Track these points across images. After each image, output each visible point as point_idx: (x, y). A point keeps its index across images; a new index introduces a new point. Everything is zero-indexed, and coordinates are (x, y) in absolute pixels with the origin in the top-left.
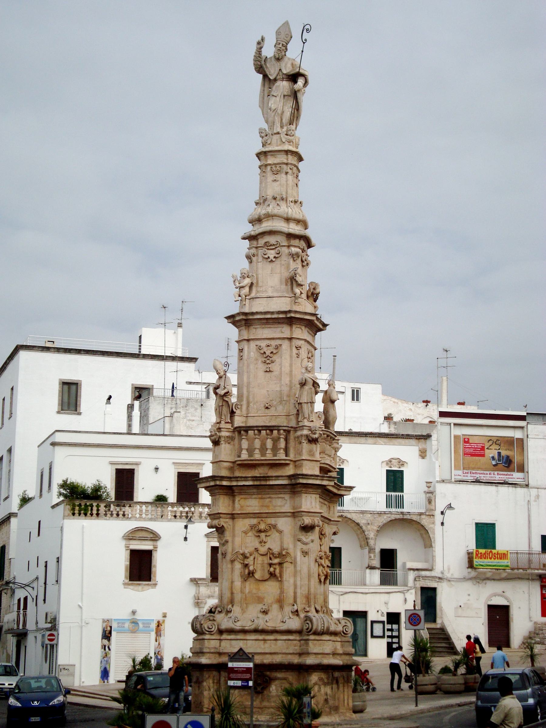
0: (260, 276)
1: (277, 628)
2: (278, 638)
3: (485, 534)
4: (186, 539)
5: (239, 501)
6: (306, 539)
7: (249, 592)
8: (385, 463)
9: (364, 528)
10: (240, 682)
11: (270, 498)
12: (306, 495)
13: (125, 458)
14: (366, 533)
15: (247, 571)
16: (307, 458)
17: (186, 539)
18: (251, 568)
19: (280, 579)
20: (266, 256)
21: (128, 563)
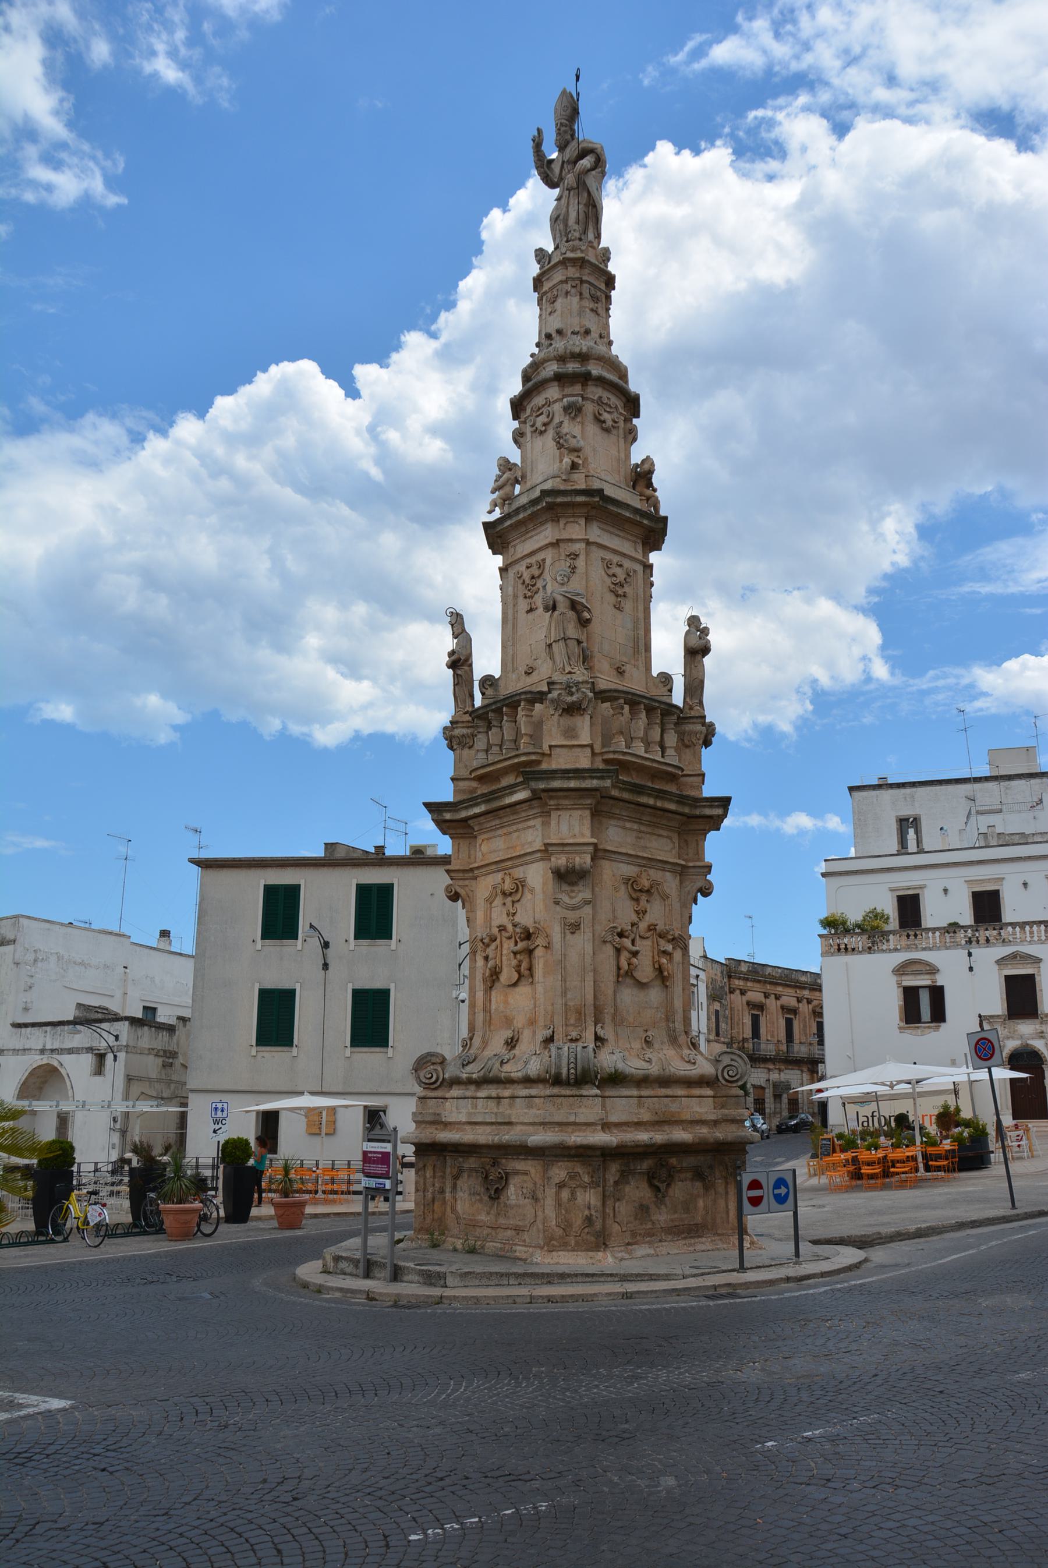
1: (512, 1075)
4: (971, 969)
6: (571, 898)
11: (517, 831)
12: (559, 813)
13: (907, 882)
16: (559, 743)
17: (971, 969)
21: (902, 1003)
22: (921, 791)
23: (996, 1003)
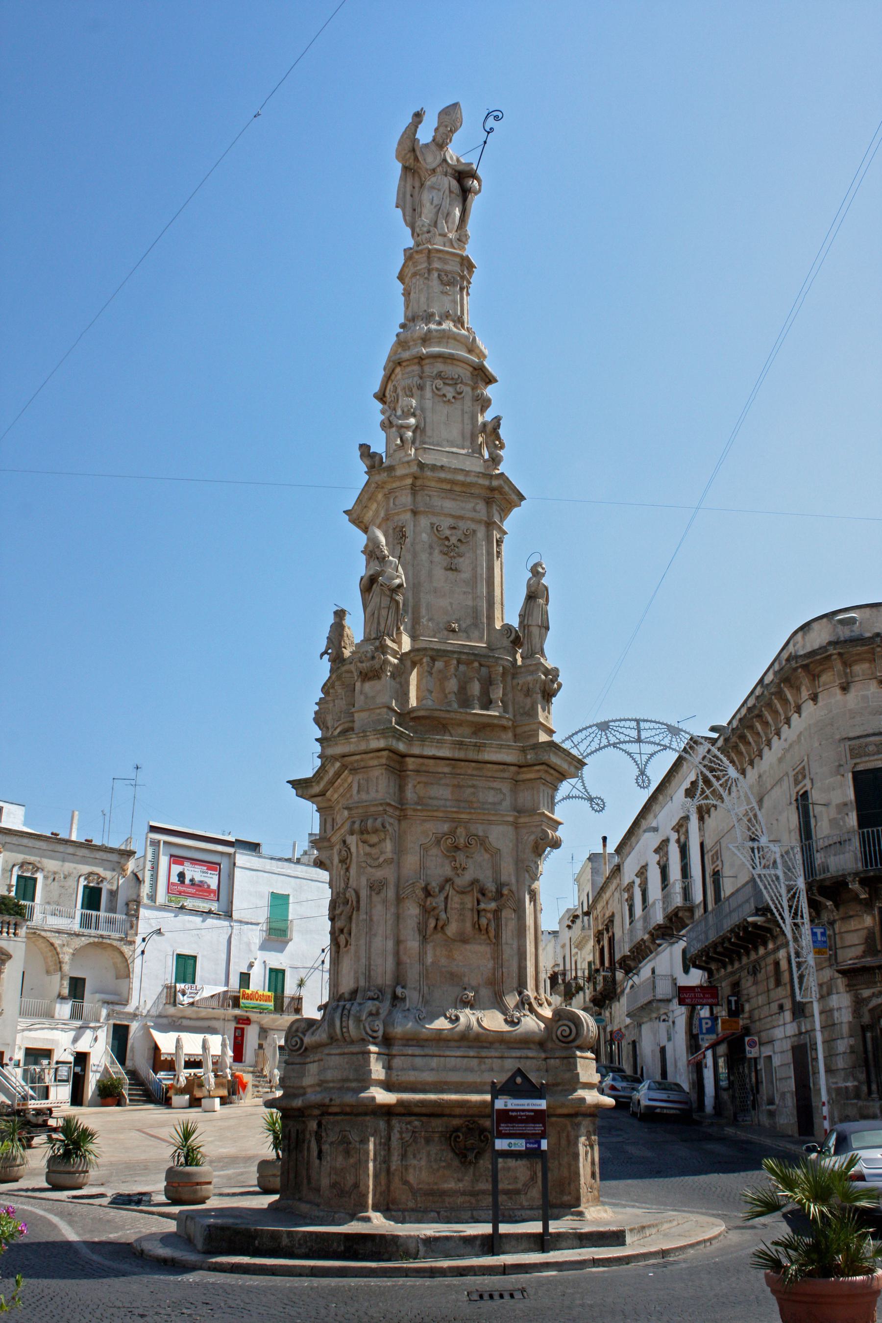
0: (428, 420)
2: (506, 1055)
5: (415, 786)
7: (432, 963)
9: (59, 949)
10: (523, 1142)
11: (473, 786)
14: (61, 956)
15: (432, 923)
18: (443, 916)
19: (494, 941)
20: (441, 393)
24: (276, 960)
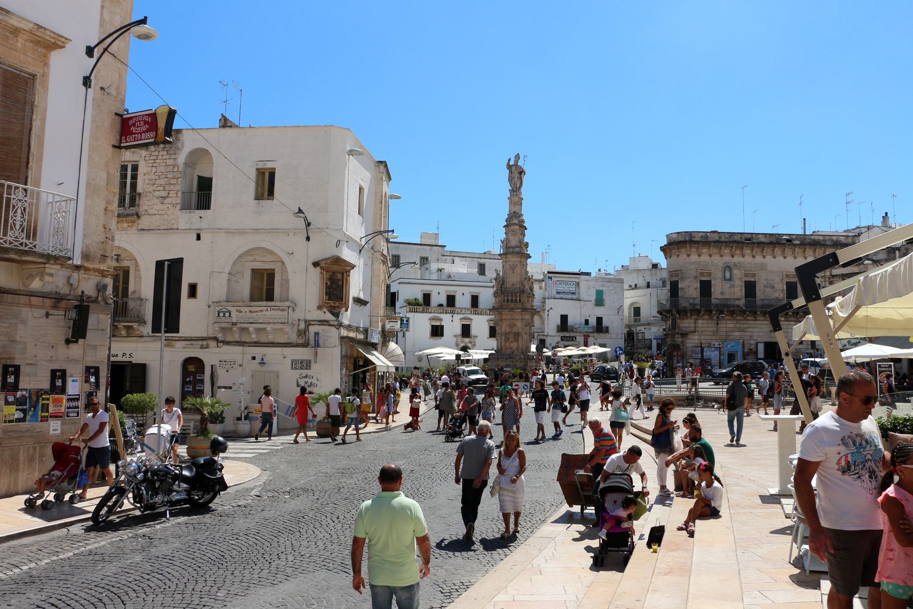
3: (564, 318)
8: (144, 222)
22: (402, 245)
23: (459, 331)
24: (599, 312)
